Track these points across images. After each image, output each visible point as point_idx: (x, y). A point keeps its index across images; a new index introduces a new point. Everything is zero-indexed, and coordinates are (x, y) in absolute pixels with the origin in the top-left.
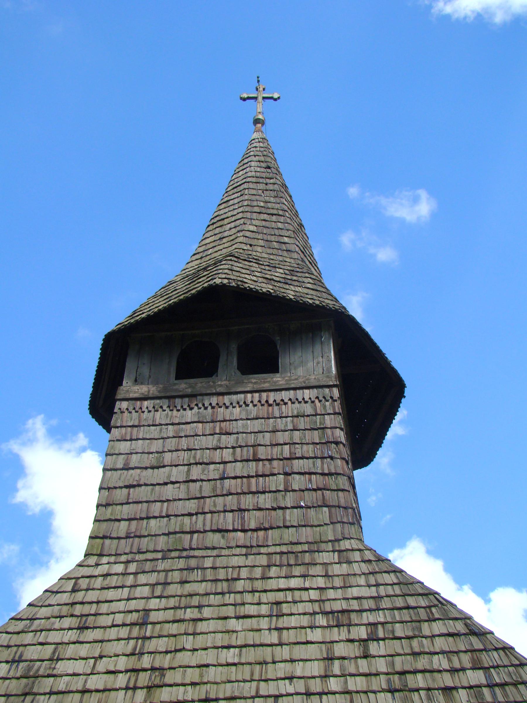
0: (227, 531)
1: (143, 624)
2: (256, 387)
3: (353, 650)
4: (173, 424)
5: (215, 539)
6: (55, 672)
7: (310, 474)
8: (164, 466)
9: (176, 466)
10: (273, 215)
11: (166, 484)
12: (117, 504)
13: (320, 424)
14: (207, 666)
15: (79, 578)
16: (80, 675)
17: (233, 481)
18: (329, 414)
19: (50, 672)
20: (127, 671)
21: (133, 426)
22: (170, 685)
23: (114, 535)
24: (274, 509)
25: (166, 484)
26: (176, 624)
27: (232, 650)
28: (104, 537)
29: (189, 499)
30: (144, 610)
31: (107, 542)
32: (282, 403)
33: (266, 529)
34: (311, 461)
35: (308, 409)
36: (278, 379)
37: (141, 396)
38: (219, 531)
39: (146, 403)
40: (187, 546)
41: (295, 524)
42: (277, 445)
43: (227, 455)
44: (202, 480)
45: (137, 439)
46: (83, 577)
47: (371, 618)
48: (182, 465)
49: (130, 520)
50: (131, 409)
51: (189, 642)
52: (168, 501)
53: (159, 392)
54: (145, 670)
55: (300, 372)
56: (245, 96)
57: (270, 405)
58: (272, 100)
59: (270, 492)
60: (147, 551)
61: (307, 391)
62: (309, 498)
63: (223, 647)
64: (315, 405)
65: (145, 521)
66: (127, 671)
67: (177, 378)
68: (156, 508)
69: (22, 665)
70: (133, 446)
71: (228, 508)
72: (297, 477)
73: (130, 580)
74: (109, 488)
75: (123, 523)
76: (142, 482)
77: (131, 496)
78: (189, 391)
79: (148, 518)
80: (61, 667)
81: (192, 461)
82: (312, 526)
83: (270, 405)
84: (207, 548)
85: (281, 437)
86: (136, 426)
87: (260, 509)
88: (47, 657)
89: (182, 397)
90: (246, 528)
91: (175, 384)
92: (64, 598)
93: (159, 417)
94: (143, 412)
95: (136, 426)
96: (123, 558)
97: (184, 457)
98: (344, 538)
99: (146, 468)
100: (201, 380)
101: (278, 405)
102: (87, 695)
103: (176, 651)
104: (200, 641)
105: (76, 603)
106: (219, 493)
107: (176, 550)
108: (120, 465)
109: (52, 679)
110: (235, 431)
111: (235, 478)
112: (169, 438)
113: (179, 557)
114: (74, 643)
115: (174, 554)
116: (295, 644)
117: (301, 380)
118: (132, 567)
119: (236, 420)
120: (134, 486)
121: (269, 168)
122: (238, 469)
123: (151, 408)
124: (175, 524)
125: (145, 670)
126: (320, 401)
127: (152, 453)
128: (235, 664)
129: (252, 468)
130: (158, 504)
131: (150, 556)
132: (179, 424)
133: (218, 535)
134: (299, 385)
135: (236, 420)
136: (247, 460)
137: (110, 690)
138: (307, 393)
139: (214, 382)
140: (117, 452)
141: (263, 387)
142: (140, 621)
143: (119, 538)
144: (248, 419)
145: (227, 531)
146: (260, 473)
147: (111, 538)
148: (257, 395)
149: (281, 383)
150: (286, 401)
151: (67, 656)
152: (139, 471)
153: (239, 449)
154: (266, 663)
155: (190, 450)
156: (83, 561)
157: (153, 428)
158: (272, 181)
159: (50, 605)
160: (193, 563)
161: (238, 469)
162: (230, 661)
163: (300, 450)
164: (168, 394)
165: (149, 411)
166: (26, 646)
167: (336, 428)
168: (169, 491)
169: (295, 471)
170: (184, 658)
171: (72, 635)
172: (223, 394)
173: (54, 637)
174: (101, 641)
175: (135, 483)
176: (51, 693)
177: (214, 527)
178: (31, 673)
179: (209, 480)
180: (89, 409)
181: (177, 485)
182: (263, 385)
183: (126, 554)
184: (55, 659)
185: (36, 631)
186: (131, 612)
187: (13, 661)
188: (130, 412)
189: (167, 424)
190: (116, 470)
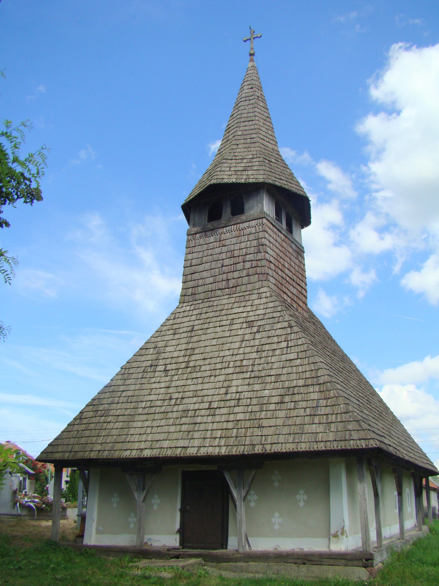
0: (223, 289)
1: (192, 331)
2: (235, 222)
3: (251, 336)
4: (206, 244)
5: (219, 293)
6: (165, 351)
7: (252, 261)
8: (203, 264)
9: (207, 263)
10: (249, 121)
11: (203, 271)
13: (257, 237)
14: (207, 346)
17: (226, 267)
19: (164, 351)
20: (184, 350)
23: (187, 295)
24: (239, 278)
25: (203, 271)
26: (201, 330)
27: (215, 339)
28: (184, 296)
31: (186, 297)
33: (236, 287)
34: (253, 255)
35: (253, 230)
36: (243, 217)
37: (195, 233)
38: (220, 289)
39: (197, 235)
42: (241, 249)
43: (224, 256)
44: (215, 268)
46: (177, 313)
47: (259, 323)
50: (192, 239)
51: (203, 337)
52: (204, 278)
54: (189, 349)
55: (252, 212)
56: (245, 39)
57: (240, 230)
58: (257, 39)
61: (253, 221)
62: (251, 271)
63: (213, 339)
66: (184, 350)
67: (208, 222)
68: (201, 282)
69: (157, 349)
70: (193, 256)
72: (247, 262)
74: (186, 275)
76: (196, 272)
79: (198, 286)
80: (168, 349)
81: (212, 260)
82: (251, 283)
83: (240, 230)
84: (216, 297)
85: (243, 245)
87: (234, 278)
88: (164, 346)
89: (210, 230)
90: (229, 287)
91: (206, 225)
92: (171, 322)
93: (202, 241)
96: (190, 303)
97: (210, 258)
98: (262, 287)
100: (215, 221)
101: (243, 230)
102: (173, 359)
105: (174, 324)
106: (221, 273)
108: (189, 265)
109: (164, 354)
110: (227, 245)
111: (226, 266)
112: (205, 250)
115: (206, 300)
116: (234, 336)
117: (251, 216)
119: (228, 239)
121: (252, 88)
123: (199, 238)
124: (206, 288)
125: (189, 349)
126: (258, 226)
128: (215, 345)
129: (232, 261)
130: (201, 280)
133: (220, 291)
134: (251, 219)
135: (228, 239)
136: (231, 258)
137: (179, 357)
138: (254, 223)
143: (189, 295)
144: (232, 238)
145: (223, 289)
146: (235, 263)
148: (235, 226)
149: (244, 219)
150: (246, 228)
151: (169, 345)
154: (224, 344)
155: (211, 255)
157: (199, 246)
159: (167, 326)
160: (211, 304)
161: (227, 262)
162: (214, 344)
165: (198, 239)
167: (263, 238)
168: (205, 274)
169: (247, 260)
170: (202, 344)
171: (171, 337)
172: (223, 227)
173: (166, 338)
175: (193, 272)
176: (163, 359)
177: (219, 288)
179: (218, 268)
181: (207, 271)
187: (155, 348)
188: (192, 240)
189: (204, 244)
190: (187, 267)
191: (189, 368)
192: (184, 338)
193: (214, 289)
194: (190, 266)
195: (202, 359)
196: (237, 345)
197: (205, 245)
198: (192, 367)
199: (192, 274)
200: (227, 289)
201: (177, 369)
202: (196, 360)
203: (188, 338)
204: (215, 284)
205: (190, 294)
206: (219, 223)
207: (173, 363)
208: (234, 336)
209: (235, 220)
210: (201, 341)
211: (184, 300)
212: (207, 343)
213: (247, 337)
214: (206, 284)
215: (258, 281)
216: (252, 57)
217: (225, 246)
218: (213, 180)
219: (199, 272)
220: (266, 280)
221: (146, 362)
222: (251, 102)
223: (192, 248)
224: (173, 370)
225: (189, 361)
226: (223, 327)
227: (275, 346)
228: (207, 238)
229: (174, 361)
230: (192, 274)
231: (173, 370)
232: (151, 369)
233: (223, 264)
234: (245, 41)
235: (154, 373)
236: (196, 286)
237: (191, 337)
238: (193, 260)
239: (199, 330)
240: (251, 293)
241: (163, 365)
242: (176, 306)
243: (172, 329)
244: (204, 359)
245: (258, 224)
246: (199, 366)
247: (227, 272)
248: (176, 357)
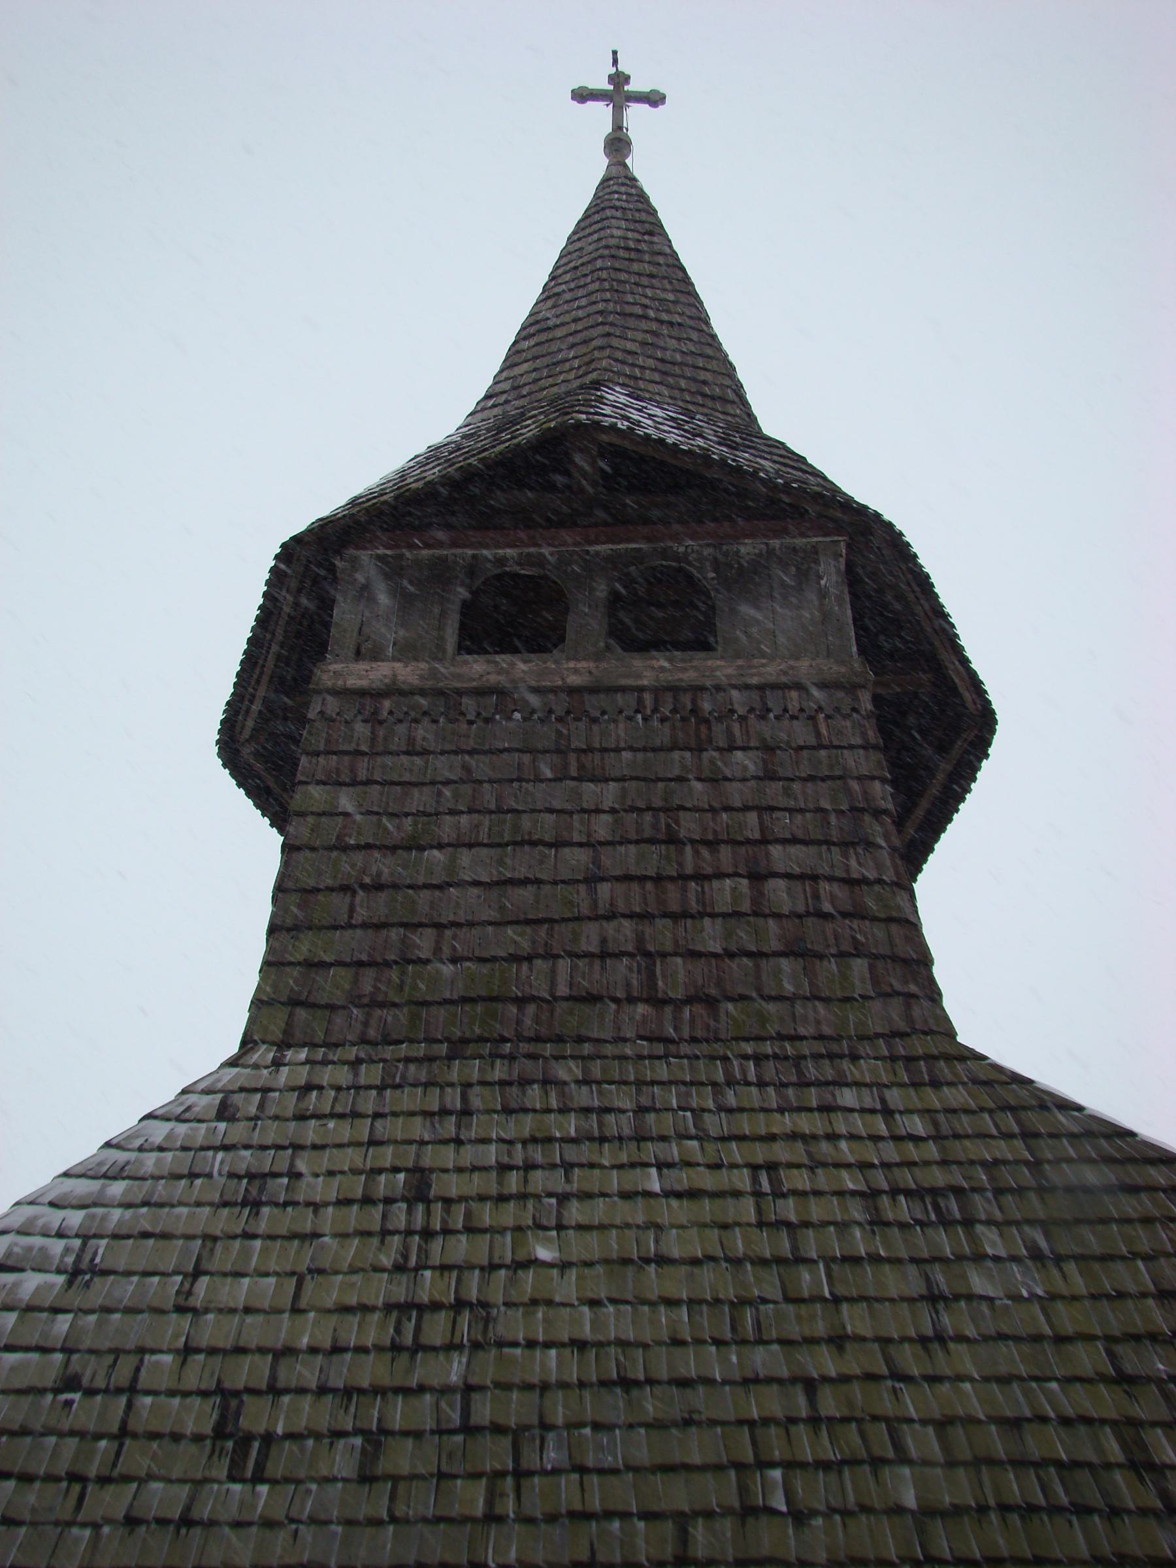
9: (470, 846)
48: (486, 845)
53: (422, 677)
67: (461, 648)
73: (370, 1101)
122: (627, 858)
141: (681, 680)
161: (627, 858)
180: (218, 742)
182: (681, 676)
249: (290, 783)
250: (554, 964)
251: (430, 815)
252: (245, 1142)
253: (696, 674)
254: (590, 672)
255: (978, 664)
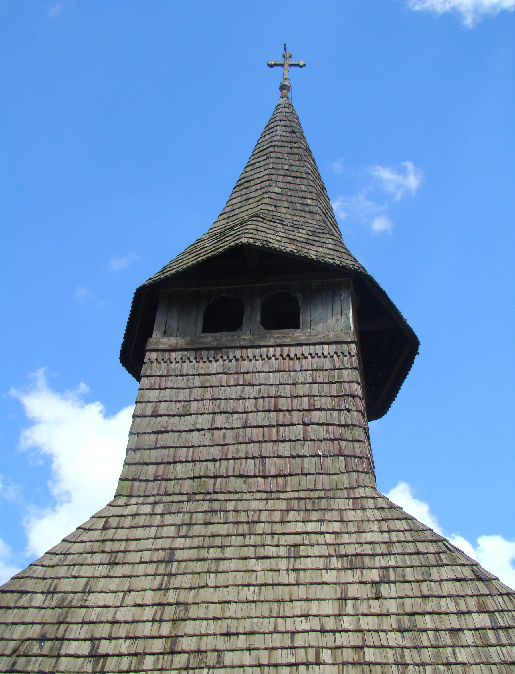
0: (249, 476)
1: (169, 561)
2: (279, 342)
3: (367, 591)
4: (199, 375)
5: (237, 484)
6: (87, 604)
7: (328, 425)
8: (190, 414)
9: (202, 414)
11: (192, 431)
12: (145, 449)
13: (338, 377)
14: (228, 602)
15: (109, 517)
16: (110, 607)
18: (347, 369)
19: (82, 603)
20: (153, 605)
21: (162, 376)
22: (194, 619)
23: (142, 478)
24: (293, 457)
28: (134, 479)
29: (213, 446)
30: (171, 549)
31: (136, 483)
32: (302, 357)
33: (285, 476)
34: (329, 412)
35: (327, 363)
36: (299, 335)
37: (170, 348)
38: (241, 476)
39: (174, 355)
40: (211, 490)
41: (313, 472)
42: (297, 396)
43: (250, 405)
44: (226, 428)
45: (166, 388)
49: (157, 464)
50: (160, 360)
51: (211, 580)
52: (193, 447)
55: (320, 328)
56: (273, 63)
57: (291, 359)
58: (298, 68)
59: (290, 441)
60: (174, 494)
61: (326, 347)
64: (334, 360)
65: (172, 465)
66: (153, 605)
67: (203, 331)
70: (162, 395)
71: (250, 455)
72: (315, 427)
73: (157, 520)
74: (138, 434)
75: (151, 466)
76: (169, 429)
77: (159, 442)
78: (215, 344)
79: (175, 462)
80: (93, 599)
81: (217, 410)
82: (329, 474)
83: (291, 359)
84: (229, 492)
85: (301, 390)
86: (164, 376)
87: (280, 457)
90: (267, 474)
91: (202, 337)
92: (96, 535)
93: (187, 367)
94: (171, 363)
95: (164, 376)
96: (151, 500)
97: (209, 406)
98: (359, 486)
99: (173, 416)
100: (225, 333)
101: (298, 359)
103: (200, 587)
104: (222, 579)
106: (241, 440)
107: (201, 493)
109: (84, 610)
110: (258, 382)
112: (195, 387)
113: (203, 500)
114: (105, 577)
115: (198, 497)
116: (311, 584)
117: (321, 336)
118: (159, 509)
119: (259, 372)
120: (162, 432)
122: (260, 418)
124: (200, 469)
126: (338, 356)
127: (179, 402)
128: (254, 602)
130: (185, 450)
131: (176, 498)
132: (205, 375)
133: (240, 480)
135: (259, 372)
136: (269, 411)
137: (137, 622)
138: (326, 349)
139: (238, 336)
140: (146, 400)
141: (285, 342)
142: (167, 559)
144: (270, 372)
145: (249, 476)
147: (140, 480)
148: (278, 349)
149: (301, 338)
150: (306, 355)
152: (166, 418)
153: (261, 400)
154: (284, 601)
156: (114, 501)
157: (180, 378)
158: (296, 145)
159: (82, 542)
160: (216, 505)
161: (260, 418)
162: (250, 598)
163: (318, 402)
164: (195, 347)
165: (177, 362)
166: (60, 578)
168: (195, 438)
169: (314, 421)
170: (206, 594)
171: (103, 570)
172: (246, 348)
173: (87, 571)
174: (130, 577)
175: (163, 429)
176: (83, 623)
178: (65, 604)
179: (232, 429)
182: (284, 340)
183: (153, 495)
184: (87, 591)
185: (70, 565)
186: (158, 550)
187: (49, 592)
188: (159, 363)
189: (194, 375)
190: (145, 416)
191: (178, 656)
192: (146, 575)
193: (223, 472)
194: (151, 416)
195: (222, 634)
196: (330, 607)
197: (196, 377)
198: (192, 652)
199: (157, 433)
200: (260, 479)
201: (136, 654)
202: (202, 635)
203: (159, 578)
204: (224, 463)
205: (152, 478)
206: (236, 337)
207: (121, 638)
208: (311, 584)
209: (278, 338)
210: (206, 589)
211: (131, 489)
212: (230, 594)
213: (353, 591)
214: (201, 461)
215: (347, 472)
216: (285, 91)
217: (253, 385)
218: (243, 238)
219: (179, 431)
220: (367, 473)
221: (23, 626)
222: (295, 151)
223: (158, 378)
224: (120, 655)
225: (177, 636)
226: (268, 561)
227: (454, 622)
228: (201, 363)
229: (122, 631)
230: (157, 433)
231: (120, 655)
232: (41, 647)
233: (246, 421)
234: (271, 66)
235: (54, 659)
236: (171, 460)
237: (170, 575)
238: (162, 404)
239: (193, 560)
240: (331, 494)
241: (85, 640)
242: (108, 502)
243: (103, 552)
244: (228, 634)
245: (339, 354)
246: (215, 650)
247: (261, 439)
248: (126, 622)
249: (141, 362)
250: (228, 463)
251: (187, 401)
252: (240, 620)
253: (290, 340)
254: (250, 340)
255: (410, 323)
